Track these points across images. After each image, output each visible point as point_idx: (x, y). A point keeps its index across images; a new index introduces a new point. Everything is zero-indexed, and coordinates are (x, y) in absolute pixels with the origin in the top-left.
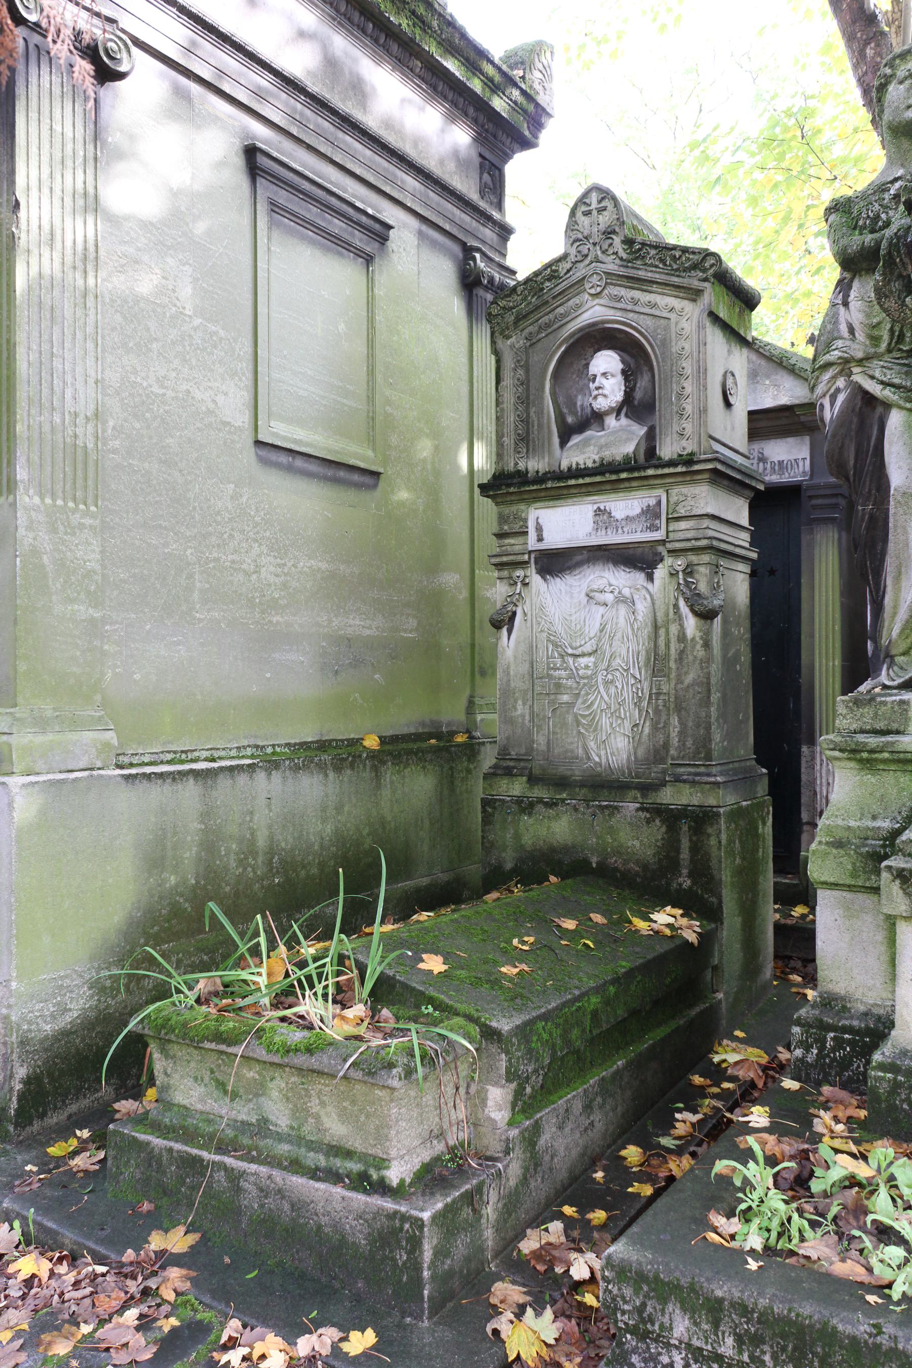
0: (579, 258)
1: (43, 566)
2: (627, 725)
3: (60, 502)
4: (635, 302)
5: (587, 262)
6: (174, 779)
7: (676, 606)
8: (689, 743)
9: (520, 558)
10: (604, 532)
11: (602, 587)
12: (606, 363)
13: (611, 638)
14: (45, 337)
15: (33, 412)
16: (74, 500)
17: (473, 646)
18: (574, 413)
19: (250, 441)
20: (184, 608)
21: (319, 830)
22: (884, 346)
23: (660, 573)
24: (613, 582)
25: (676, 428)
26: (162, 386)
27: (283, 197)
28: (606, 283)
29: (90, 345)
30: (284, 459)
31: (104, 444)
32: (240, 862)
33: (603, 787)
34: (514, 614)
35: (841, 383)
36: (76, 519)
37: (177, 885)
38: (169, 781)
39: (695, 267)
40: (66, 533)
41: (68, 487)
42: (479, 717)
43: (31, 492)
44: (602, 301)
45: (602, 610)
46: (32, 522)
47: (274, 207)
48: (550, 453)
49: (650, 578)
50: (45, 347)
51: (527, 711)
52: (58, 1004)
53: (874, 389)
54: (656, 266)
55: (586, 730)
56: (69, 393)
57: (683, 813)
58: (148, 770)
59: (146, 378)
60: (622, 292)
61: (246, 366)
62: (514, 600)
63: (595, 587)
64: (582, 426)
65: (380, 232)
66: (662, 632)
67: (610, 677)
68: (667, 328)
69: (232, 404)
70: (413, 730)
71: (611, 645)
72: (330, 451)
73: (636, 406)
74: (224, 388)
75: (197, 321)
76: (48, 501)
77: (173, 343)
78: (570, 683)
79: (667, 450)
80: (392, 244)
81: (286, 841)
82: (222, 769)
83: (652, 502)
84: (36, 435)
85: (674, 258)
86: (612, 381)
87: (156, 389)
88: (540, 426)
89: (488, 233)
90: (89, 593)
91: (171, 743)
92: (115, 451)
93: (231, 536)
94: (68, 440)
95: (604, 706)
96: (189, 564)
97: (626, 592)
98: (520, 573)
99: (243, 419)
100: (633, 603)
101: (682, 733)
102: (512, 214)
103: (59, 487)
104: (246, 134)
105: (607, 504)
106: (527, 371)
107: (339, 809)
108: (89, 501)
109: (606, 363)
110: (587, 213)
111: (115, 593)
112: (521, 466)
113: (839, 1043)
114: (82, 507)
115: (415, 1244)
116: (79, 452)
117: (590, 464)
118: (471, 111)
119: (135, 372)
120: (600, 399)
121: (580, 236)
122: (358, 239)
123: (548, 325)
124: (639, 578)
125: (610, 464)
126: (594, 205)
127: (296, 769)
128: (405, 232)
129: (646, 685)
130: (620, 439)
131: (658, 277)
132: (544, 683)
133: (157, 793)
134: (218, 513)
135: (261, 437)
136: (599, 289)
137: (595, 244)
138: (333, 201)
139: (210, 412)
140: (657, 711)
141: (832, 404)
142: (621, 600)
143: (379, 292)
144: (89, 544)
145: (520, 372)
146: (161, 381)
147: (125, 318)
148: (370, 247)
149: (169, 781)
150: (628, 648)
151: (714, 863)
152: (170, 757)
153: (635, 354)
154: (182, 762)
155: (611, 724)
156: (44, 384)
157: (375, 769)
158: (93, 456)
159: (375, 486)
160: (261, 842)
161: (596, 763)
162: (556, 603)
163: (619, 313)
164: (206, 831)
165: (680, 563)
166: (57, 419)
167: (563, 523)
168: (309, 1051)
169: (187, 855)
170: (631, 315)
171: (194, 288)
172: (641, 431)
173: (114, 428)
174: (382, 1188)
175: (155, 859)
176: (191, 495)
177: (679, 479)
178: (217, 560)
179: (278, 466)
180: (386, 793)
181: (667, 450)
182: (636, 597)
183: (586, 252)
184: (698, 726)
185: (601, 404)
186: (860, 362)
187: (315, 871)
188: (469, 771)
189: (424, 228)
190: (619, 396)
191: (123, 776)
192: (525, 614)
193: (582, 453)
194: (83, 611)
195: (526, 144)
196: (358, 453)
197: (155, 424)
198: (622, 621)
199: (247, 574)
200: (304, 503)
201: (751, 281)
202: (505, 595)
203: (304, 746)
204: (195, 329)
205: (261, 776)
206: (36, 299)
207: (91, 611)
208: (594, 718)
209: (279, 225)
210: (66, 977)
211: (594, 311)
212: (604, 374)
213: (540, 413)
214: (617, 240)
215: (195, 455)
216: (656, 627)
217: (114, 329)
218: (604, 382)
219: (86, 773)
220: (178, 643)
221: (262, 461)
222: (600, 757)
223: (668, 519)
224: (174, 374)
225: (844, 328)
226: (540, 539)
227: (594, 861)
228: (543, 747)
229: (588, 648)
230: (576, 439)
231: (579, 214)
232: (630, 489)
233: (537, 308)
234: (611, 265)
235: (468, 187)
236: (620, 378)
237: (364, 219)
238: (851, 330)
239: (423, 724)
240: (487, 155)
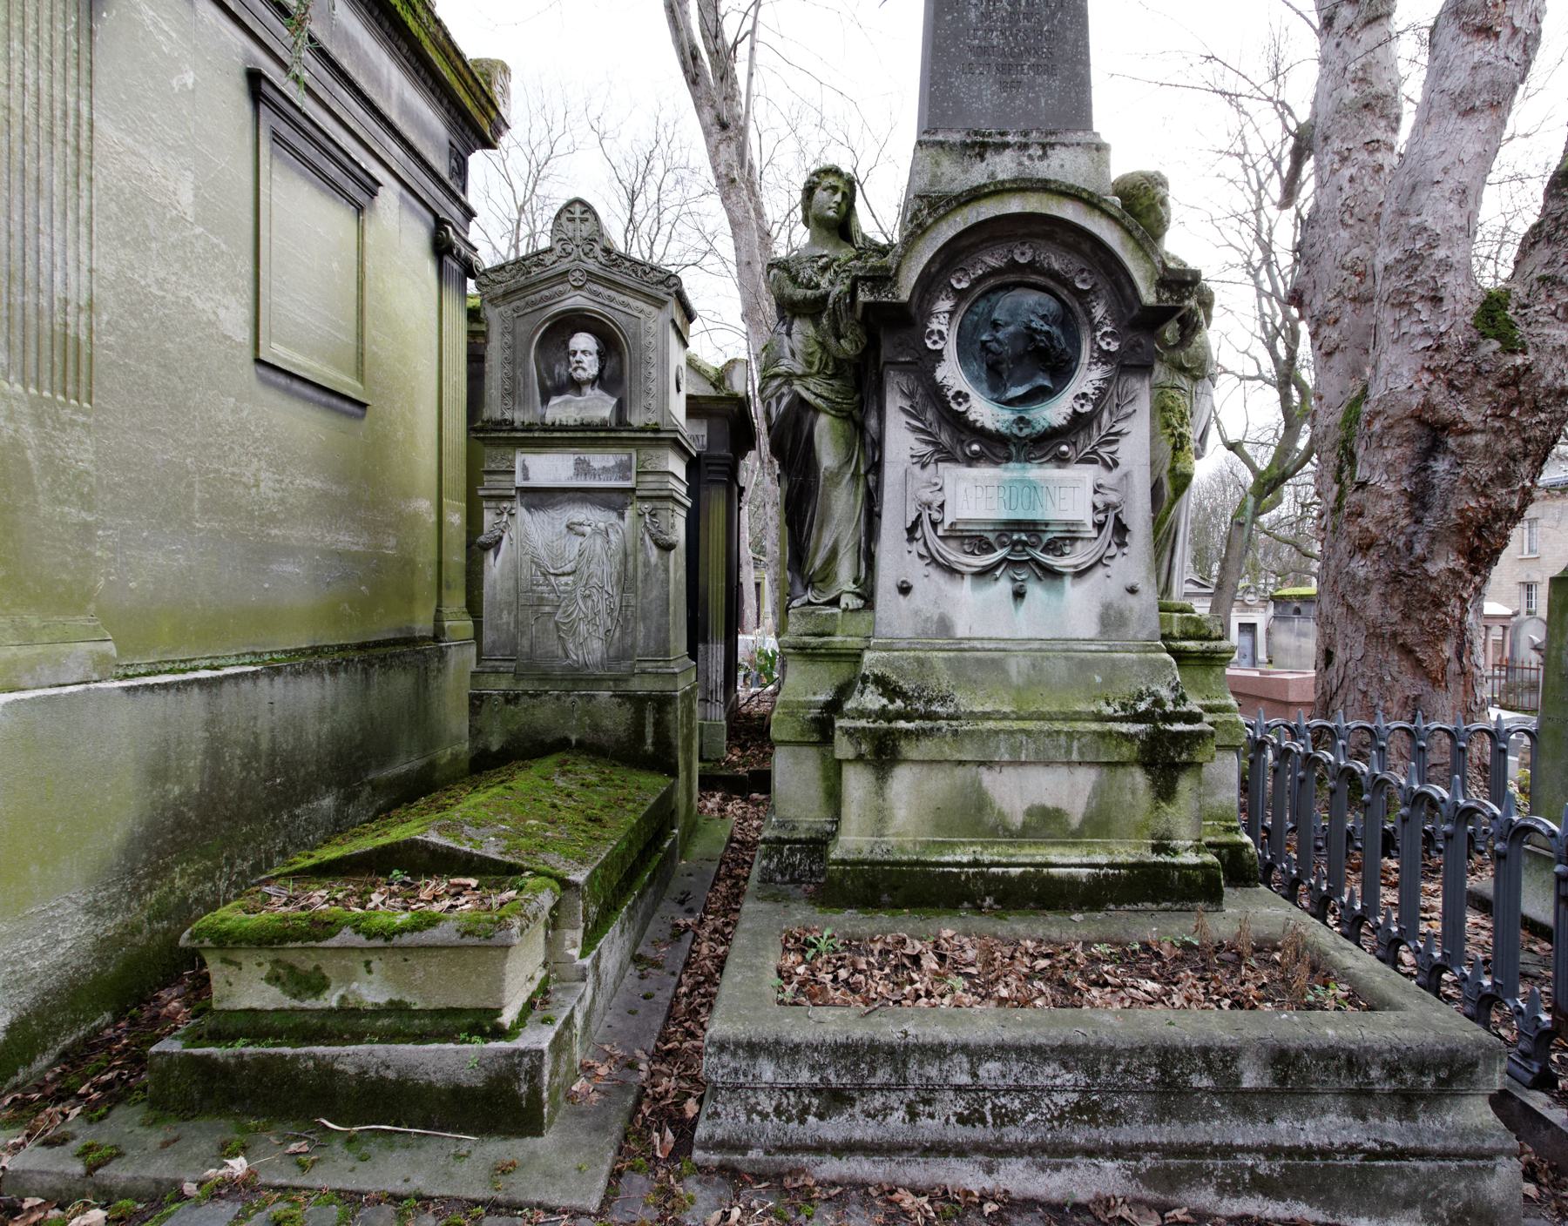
1: (26, 462)
2: (601, 630)
3: (46, 394)
6: (178, 689)
7: (642, 539)
8: (652, 644)
12: (583, 342)
13: (589, 562)
14: (30, 209)
15: (14, 289)
16: (65, 393)
17: (440, 563)
18: (552, 377)
19: (248, 355)
20: (183, 516)
21: (315, 731)
22: (815, 368)
23: (629, 513)
25: (644, 403)
26: (161, 288)
27: (285, 130)
29: (83, 230)
30: (282, 380)
31: (99, 339)
32: (244, 767)
33: (579, 678)
35: (785, 389)
36: (66, 414)
37: (181, 795)
38: (173, 691)
39: (662, 282)
40: (54, 428)
41: (57, 378)
42: (447, 624)
43: (12, 378)
45: (580, 539)
46: (12, 412)
47: (276, 137)
48: (534, 409)
49: (622, 516)
50: (30, 221)
51: (512, 620)
52: (49, 937)
53: (805, 394)
56: (58, 277)
57: (649, 697)
58: (151, 680)
59: (144, 277)
60: (601, 289)
61: (246, 284)
64: (560, 390)
65: (371, 187)
66: (631, 559)
68: (638, 325)
69: (234, 319)
70: (392, 636)
72: (326, 379)
73: (609, 380)
74: (225, 302)
75: (199, 230)
76: (32, 391)
77: (174, 246)
78: (552, 596)
79: (637, 419)
80: (378, 200)
81: (286, 742)
82: (227, 677)
84: (18, 317)
85: (645, 273)
87: (154, 290)
88: (526, 386)
89: (455, 211)
90: (81, 495)
91: (170, 652)
92: (109, 347)
93: (232, 449)
94: (57, 328)
96: (188, 472)
97: (602, 525)
99: (244, 336)
101: (647, 636)
102: (473, 199)
103: (45, 377)
104: (250, 58)
106: (514, 338)
107: (334, 710)
108: (83, 396)
109: (583, 342)
110: (572, 220)
111: (109, 497)
112: (508, 416)
113: (792, 852)
114: (73, 402)
115: (535, 1073)
116: (70, 343)
117: (571, 422)
118: (445, 102)
119: (132, 268)
120: (580, 371)
122: (351, 187)
123: (534, 303)
124: (612, 517)
125: (589, 425)
126: (578, 215)
127: (297, 673)
128: (390, 192)
129: (617, 600)
130: (597, 406)
131: (631, 284)
132: (531, 601)
133: (158, 704)
134: (219, 425)
135: (262, 356)
138: (331, 147)
139: (210, 323)
140: (626, 619)
141: (778, 403)
142: (596, 532)
143: (368, 240)
144: (82, 443)
145: (508, 338)
146: (160, 283)
147: (121, 209)
148: (362, 198)
149: (173, 691)
150: (604, 571)
151: (672, 734)
152: (167, 667)
153: (610, 344)
154: (183, 671)
156: (28, 262)
157: (365, 671)
158: (85, 350)
159: (363, 416)
160: (264, 745)
162: (535, 532)
164: (213, 739)
165: (647, 506)
166: (44, 302)
167: (548, 468)
168: (415, 928)
169: (192, 764)
171: (195, 196)
172: (614, 401)
173: (108, 323)
174: (499, 1033)
175: (158, 774)
176: (190, 403)
178: (218, 471)
179: (277, 386)
180: (374, 692)
181: (637, 419)
184: (659, 630)
185: (580, 375)
186: (800, 377)
187: (313, 768)
188: (439, 670)
189: (405, 192)
190: (593, 371)
191: (123, 688)
193: (562, 410)
194: (75, 514)
195: (488, 144)
196: (346, 383)
197: (154, 326)
198: (598, 548)
199: (246, 486)
200: (304, 424)
201: (695, 305)
203: (300, 652)
204: (197, 237)
205: (263, 683)
206: (18, 165)
207: (83, 514)
209: (280, 156)
210: (58, 906)
211: (576, 300)
212: (583, 352)
213: (526, 374)
214: (597, 248)
215: (195, 364)
216: (626, 555)
217: (108, 218)
218: (583, 358)
219: (82, 687)
220: (178, 552)
221: (261, 379)
224: (174, 278)
225: (787, 351)
226: (526, 478)
227: (574, 738)
228: (527, 649)
229: (568, 568)
230: (555, 400)
231: (563, 220)
232: (607, 446)
233: (526, 287)
234: (592, 266)
235: (442, 166)
236: (595, 356)
237: (357, 171)
238: (793, 354)
239: (400, 630)
240: (455, 143)
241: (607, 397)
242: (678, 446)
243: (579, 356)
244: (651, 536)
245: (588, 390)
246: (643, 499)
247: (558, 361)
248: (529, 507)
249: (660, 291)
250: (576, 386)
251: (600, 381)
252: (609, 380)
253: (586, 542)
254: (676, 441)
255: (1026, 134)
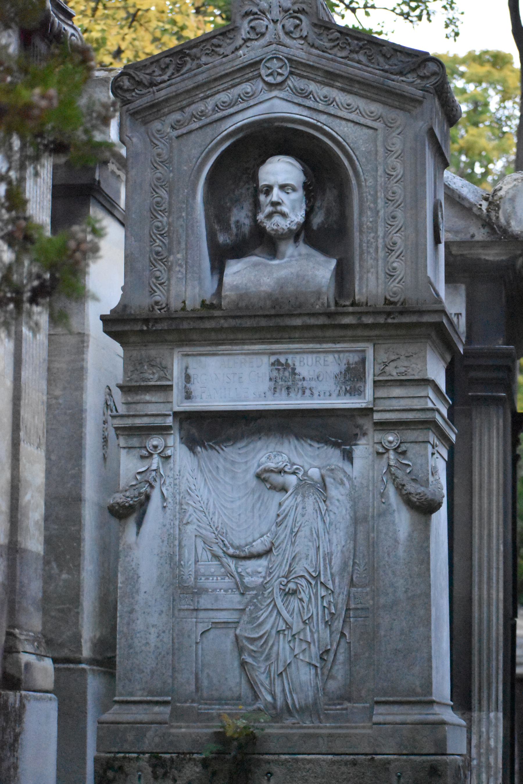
0: (253, 36)
2: (314, 649)
4: (329, 101)
5: (263, 41)
9: (158, 421)
10: (284, 392)
11: (281, 465)
12: (281, 171)
13: (294, 534)
23: (362, 450)
24: (297, 460)
28: (291, 73)
34: (148, 497)
44: (282, 94)
45: (278, 497)
49: (349, 457)
54: (359, 62)
55: (254, 658)
62: (147, 481)
63: (272, 465)
64: (238, 250)
67: (292, 586)
71: (293, 543)
83: (354, 358)
86: (294, 196)
95: (282, 626)
97: (314, 473)
98: (156, 441)
100: (325, 486)
105: (290, 357)
109: (281, 171)
120: (277, 219)
121: (255, 10)
124: (333, 456)
129: (341, 599)
136: (279, 79)
137: (275, 22)
142: (305, 485)
153: (325, 170)
155: (292, 650)
161: (266, 702)
163: (306, 112)
167: (228, 380)
170: (323, 118)
172: (333, 263)
177: (393, 332)
182: (328, 480)
183: (263, 30)
185: (278, 224)
190: (297, 217)
192: (164, 498)
202: (134, 472)
208: (266, 642)
211: (278, 106)
212: (283, 187)
222: (274, 697)
223: (375, 382)
226: (188, 396)
234: (297, 49)
241: (321, 258)
242: (440, 334)
243: (276, 194)
244: (400, 488)
245: (289, 249)
246: (383, 426)
247: (236, 201)
248: (191, 443)
249: (409, 85)
250: (263, 242)
251: (306, 234)
252: (328, 232)
253: (289, 501)
254: (439, 327)
255: (356, 621)
